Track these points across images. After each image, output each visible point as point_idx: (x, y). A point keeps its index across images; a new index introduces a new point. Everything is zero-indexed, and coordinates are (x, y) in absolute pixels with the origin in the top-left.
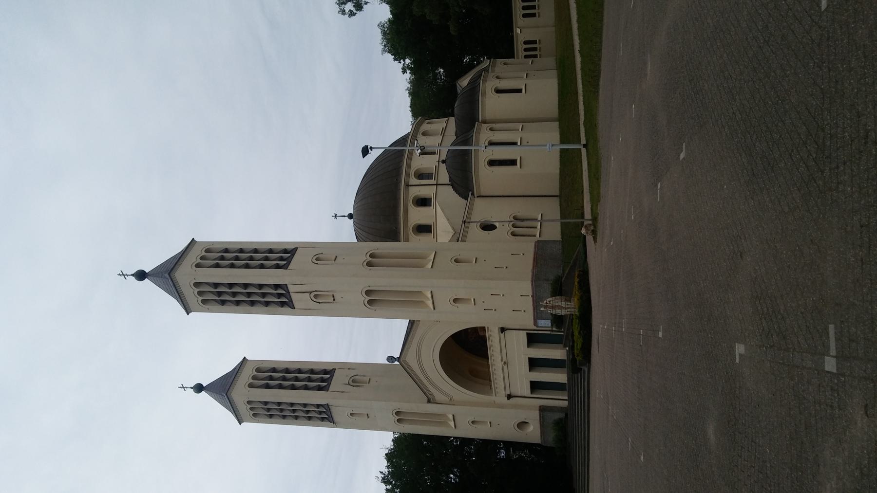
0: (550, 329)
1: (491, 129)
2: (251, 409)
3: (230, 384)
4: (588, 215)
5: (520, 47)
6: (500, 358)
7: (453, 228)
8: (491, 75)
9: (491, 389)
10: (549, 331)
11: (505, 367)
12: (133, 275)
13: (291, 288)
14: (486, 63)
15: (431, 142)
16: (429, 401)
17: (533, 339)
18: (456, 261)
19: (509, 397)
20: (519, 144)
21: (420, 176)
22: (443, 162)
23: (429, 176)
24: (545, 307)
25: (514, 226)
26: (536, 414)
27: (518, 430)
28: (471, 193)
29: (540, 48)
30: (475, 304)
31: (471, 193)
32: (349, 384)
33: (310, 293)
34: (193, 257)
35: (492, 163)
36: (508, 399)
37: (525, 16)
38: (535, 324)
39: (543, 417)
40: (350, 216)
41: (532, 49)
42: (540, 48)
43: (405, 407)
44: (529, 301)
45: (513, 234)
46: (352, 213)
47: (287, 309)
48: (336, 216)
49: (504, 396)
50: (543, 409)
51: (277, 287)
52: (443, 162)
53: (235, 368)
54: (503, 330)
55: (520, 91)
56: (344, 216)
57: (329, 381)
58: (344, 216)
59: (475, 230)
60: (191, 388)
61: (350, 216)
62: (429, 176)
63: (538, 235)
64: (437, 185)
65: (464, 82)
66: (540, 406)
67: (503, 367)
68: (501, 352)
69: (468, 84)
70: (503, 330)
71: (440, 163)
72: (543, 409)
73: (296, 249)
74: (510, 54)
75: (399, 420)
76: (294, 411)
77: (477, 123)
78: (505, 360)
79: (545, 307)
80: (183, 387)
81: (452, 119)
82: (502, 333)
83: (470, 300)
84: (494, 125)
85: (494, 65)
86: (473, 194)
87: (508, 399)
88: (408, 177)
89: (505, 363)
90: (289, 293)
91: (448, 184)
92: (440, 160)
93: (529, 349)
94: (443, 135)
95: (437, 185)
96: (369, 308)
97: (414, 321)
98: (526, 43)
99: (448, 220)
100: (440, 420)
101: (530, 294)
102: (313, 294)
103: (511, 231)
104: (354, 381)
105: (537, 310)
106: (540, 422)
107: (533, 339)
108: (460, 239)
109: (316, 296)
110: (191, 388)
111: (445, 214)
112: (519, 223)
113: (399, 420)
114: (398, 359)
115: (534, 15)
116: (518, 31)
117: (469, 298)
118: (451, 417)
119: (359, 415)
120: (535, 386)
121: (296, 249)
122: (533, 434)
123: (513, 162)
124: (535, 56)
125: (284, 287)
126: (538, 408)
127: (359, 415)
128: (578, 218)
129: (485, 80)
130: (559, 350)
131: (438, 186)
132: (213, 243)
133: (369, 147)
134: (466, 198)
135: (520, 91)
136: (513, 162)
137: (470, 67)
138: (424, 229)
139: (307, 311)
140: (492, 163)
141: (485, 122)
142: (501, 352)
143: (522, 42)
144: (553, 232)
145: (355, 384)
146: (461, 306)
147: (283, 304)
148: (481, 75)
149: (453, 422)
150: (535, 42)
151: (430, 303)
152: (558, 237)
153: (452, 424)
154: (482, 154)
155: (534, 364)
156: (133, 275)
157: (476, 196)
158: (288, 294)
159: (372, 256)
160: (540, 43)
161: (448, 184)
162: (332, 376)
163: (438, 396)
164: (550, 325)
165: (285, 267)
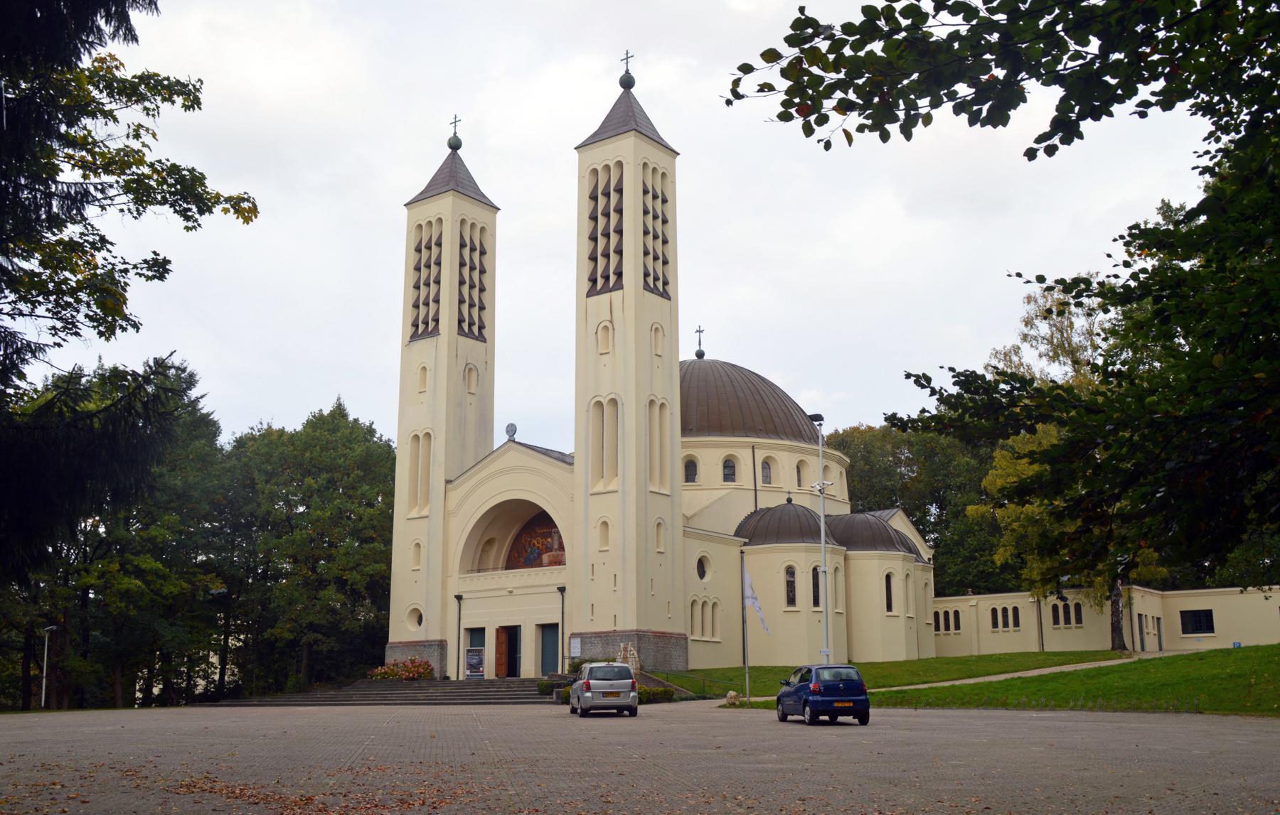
0: (566, 654)
1: (836, 569)
2: (430, 223)
3: (466, 192)
4: (753, 699)
5: (951, 604)
6: (518, 585)
7: (695, 515)
8: (911, 566)
9: (468, 572)
10: (563, 654)
11: (505, 593)
12: (627, 72)
13: (617, 295)
14: (927, 553)
15: (813, 478)
16: (448, 482)
17: (549, 631)
18: (659, 524)
19: (459, 598)
20: (889, 613)
21: (767, 464)
22: (789, 500)
23: (767, 479)
24: (625, 649)
25: (704, 604)
26: (435, 636)
27: (409, 610)
28: (747, 540)
29: (949, 634)
30: (600, 551)
31: (747, 540)
32: (467, 365)
33: (611, 322)
34: (656, 157)
35: (790, 571)
36: (456, 597)
37: (994, 611)
38: (573, 635)
39: (432, 645)
40: (700, 355)
41: (946, 623)
42: (949, 634)
43: (439, 445)
44: (608, 627)
45: (694, 603)
46: (705, 358)
47: (586, 285)
48: (700, 331)
49: (462, 590)
50: (442, 645)
51: (619, 275)
52: (789, 500)
53: (483, 196)
54: (562, 590)
55: (889, 608)
56: (700, 344)
57: (470, 335)
58: (700, 344)
59: (697, 549)
60: (455, 133)
61: (700, 355)
62: (767, 479)
63: (693, 638)
64: (756, 490)
65: (899, 522)
66: (446, 641)
67: (505, 589)
68: (527, 587)
69: (895, 530)
70: (562, 590)
71: (787, 496)
72: (442, 645)
73: (669, 299)
74: (939, 593)
75: (416, 437)
76: (427, 284)
77: (845, 548)
78: (515, 592)
79: (625, 649)
80: (455, 122)
81: (845, 510)
82: (558, 588)
83: (607, 544)
84: (841, 574)
85: (924, 569)
86: (745, 544)
87: (456, 597)
88: (767, 446)
89: (511, 592)
90: (610, 291)
91: (756, 506)
92: (791, 496)
93: (534, 626)
94: (624, 476)
95: (756, 490)
96: (590, 403)
97: (571, 464)
98: (957, 613)
99: (707, 507)
100: (421, 493)
101: (618, 628)
102: (607, 324)
103: (707, 600)
104: (470, 369)
105: (595, 637)
106: (423, 642)
107: (549, 631)
108: (687, 529)
109: (608, 328)
110: (455, 133)
111: (714, 503)
112: (708, 609)
113: (416, 437)
114: (512, 440)
115: (995, 625)
116: (973, 602)
117: (610, 542)
118: (425, 513)
119: (424, 381)
120: (477, 634)
121: (669, 299)
122: (401, 630)
123: (791, 600)
124: (937, 628)
125: (619, 286)
126: (444, 639)
127: (424, 381)
128: (750, 691)
129: (904, 559)
130: (534, 668)
131: (753, 492)
132: (674, 182)
133: (822, 422)
134: (737, 534)
135: (889, 608)
136: (791, 600)
137: (922, 526)
138: (691, 469)
139: (583, 316)
140: (790, 571)
141: (846, 558)
142: (527, 587)
143: (957, 609)
144: (700, 659)
145: (467, 371)
146: (596, 533)
147: (593, 281)
148: (911, 551)
149: (417, 516)
150: (957, 627)
151: (599, 487)
152: (693, 665)
153: (414, 514)
154: (802, 556)
155: (510, 636)
156: (627, 72)
157: (744, 548)
158: (606, 289)
159: (662, 405)
160: (955, 634)
161: (756, 506)
162: (476, 339)
163: (456, 495)
164: (573, 655)
165: (461, 331)
